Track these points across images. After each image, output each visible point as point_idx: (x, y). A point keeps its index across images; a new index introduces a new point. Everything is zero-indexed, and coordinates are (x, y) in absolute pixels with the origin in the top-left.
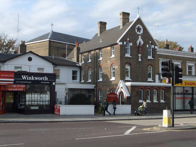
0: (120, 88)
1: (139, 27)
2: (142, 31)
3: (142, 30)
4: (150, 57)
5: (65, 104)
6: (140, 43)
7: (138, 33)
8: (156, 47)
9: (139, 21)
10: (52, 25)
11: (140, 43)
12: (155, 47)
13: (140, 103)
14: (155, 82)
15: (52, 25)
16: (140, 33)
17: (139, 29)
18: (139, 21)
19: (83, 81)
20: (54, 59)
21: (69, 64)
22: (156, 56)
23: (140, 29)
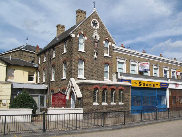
0: (71, 88)
1: (95, 21)
2: (98, 27)
3: (98, 24)
4: (107, 55)
5: (169, 96)
6: (96, 37)
7: (94, 27)
8: (113, 45)
9: (94, 15)
10: (27, 39)
11: (96, 37)
12: (111, 45)
13: (95, 105)
14: (112, 81)
15: (27, 39)
16: (96, 28)
17: (95, 24)
18: (94, 15)
19: (39, 82)
20: (11, 60)
21: (26, 65)
22: (113, 54)
23: (96, 24)
